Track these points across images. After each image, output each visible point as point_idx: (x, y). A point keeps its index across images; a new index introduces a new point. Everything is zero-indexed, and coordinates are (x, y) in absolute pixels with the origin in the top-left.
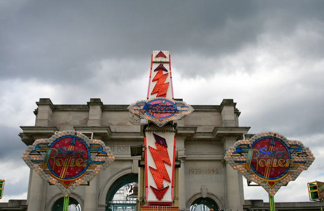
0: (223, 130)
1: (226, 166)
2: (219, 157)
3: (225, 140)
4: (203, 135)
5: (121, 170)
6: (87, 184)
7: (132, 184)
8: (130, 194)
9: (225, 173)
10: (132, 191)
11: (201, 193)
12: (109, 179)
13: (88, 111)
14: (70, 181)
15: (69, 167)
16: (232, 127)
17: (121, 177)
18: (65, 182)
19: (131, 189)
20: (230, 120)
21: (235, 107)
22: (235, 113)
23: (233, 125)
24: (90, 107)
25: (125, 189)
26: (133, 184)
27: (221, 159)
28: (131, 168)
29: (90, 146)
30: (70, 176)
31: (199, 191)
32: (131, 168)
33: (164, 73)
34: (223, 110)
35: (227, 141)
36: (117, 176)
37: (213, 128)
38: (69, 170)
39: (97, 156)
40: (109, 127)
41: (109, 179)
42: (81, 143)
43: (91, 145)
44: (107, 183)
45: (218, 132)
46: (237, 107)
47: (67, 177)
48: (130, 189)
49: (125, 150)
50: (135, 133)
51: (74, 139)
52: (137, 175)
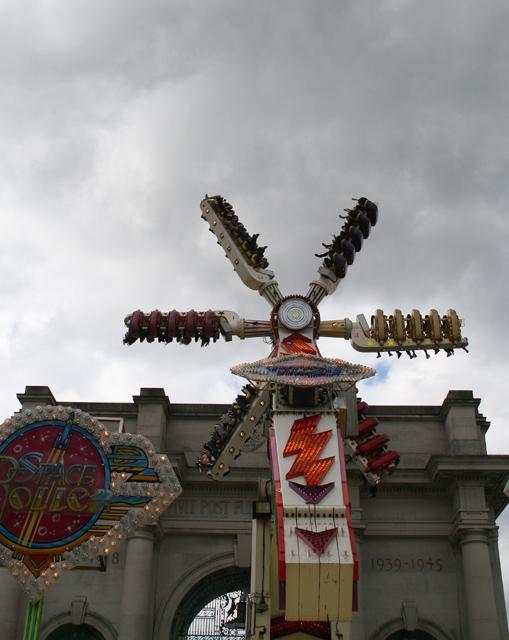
0: (452, 463)
1: (460, 549)
2: (444, 529)
3: (457, 488)
4: (405, 476)
5: (208, 558)
6: (97, 564)
7: (234, 595)
8: (230, 618)
9: (460, 569)
10: (235, 611)
11: (69, 613)
12: (180, 582)
13: (135, 418)
14: (46, 555)
15: (46, 510)
16: (473, 456)
17: (208, 577)
18: (33, 557)
19: (233, 607)
20: (467, 440)
21: (477, 411)
22: (478, 423)
23: (475, 452)
24: (140, 406)
25: (218, 608)
26: (236, 595)
27: (446, 533)
28: (232, 554)
29: (110, 451)
30: (48, 539)
31: (396, 614)
32: (232, 554)
33: (301, 481)
34: (450, 415)
35: (461, 490)
36: (204, 570)
37: (427, 461)
38: (46, 520)
39: (128, 481)
40: (183, 454)
41: (180, 582)
42: (87, 442)
43: (113, 447)
44: (175, 589)
45: (440, 467)
46: (481, 410)
47: (38, 539)
48: (230, 605)
49: (218, 510)
50: (243, 469)
51: (67, 430)
52: (247, 572)
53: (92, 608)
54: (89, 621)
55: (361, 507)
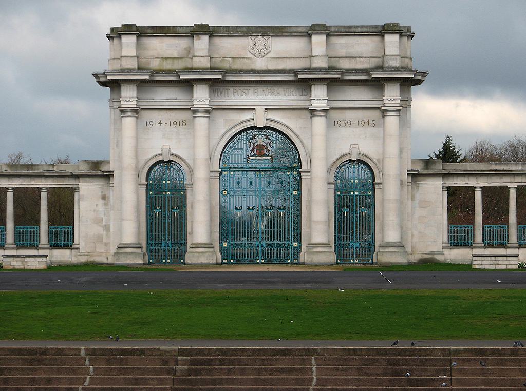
5: (239, 122)
8: (252, 154)
10: (255, 150)
12: (223, 136)
19: (254, 148)
31: (347, 151)
41: (223, 136)
48: (252, 147)
53: (173, 152)
54: (172, 158)
55: (327, 97)
